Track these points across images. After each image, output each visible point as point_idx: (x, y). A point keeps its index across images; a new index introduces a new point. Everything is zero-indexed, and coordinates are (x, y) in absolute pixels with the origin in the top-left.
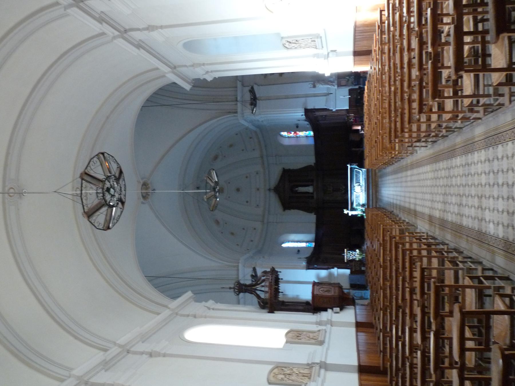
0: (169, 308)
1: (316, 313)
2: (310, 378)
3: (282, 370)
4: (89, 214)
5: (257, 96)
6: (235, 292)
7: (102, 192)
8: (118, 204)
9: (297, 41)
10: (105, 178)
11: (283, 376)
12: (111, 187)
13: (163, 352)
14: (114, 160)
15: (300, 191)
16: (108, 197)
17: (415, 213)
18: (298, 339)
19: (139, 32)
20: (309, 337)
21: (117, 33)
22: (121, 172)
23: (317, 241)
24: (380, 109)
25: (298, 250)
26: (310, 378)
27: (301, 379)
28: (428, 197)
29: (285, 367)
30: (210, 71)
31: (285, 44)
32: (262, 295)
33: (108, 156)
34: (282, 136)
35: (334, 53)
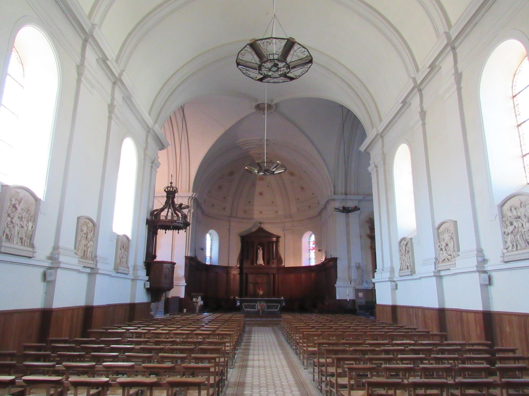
0: (154, 125)
1: (145, 266)
2: (82, 258)
3: (91, 231)
4: (254, 46)
5: (351, 214)
6: (167, 187)
7: (274, 58)
8: (262, 74)
9: (408, 252)
10: (288, 63)
11: (85, 232)
12: (279, 68)
13: (113, 116)
14: (303, 73)
15: (258, 252)
16: (269, 65)
17: (244, 367)
18: (121, 247)
19: (419, 103)
20: (122, 258)
21: (419, 82)
22: (292, 79)
23: (211, 267)
24: (317, 327)
25: (203, 249)
26: (82, 258)
27: (82, 250)
28: (263, 381)
29: (94, 234)
30: (378, 169)
31: (405, 241)
32: (164, 214)
33: (309, 66)
34: (311, 236)
35: (395, 288)
